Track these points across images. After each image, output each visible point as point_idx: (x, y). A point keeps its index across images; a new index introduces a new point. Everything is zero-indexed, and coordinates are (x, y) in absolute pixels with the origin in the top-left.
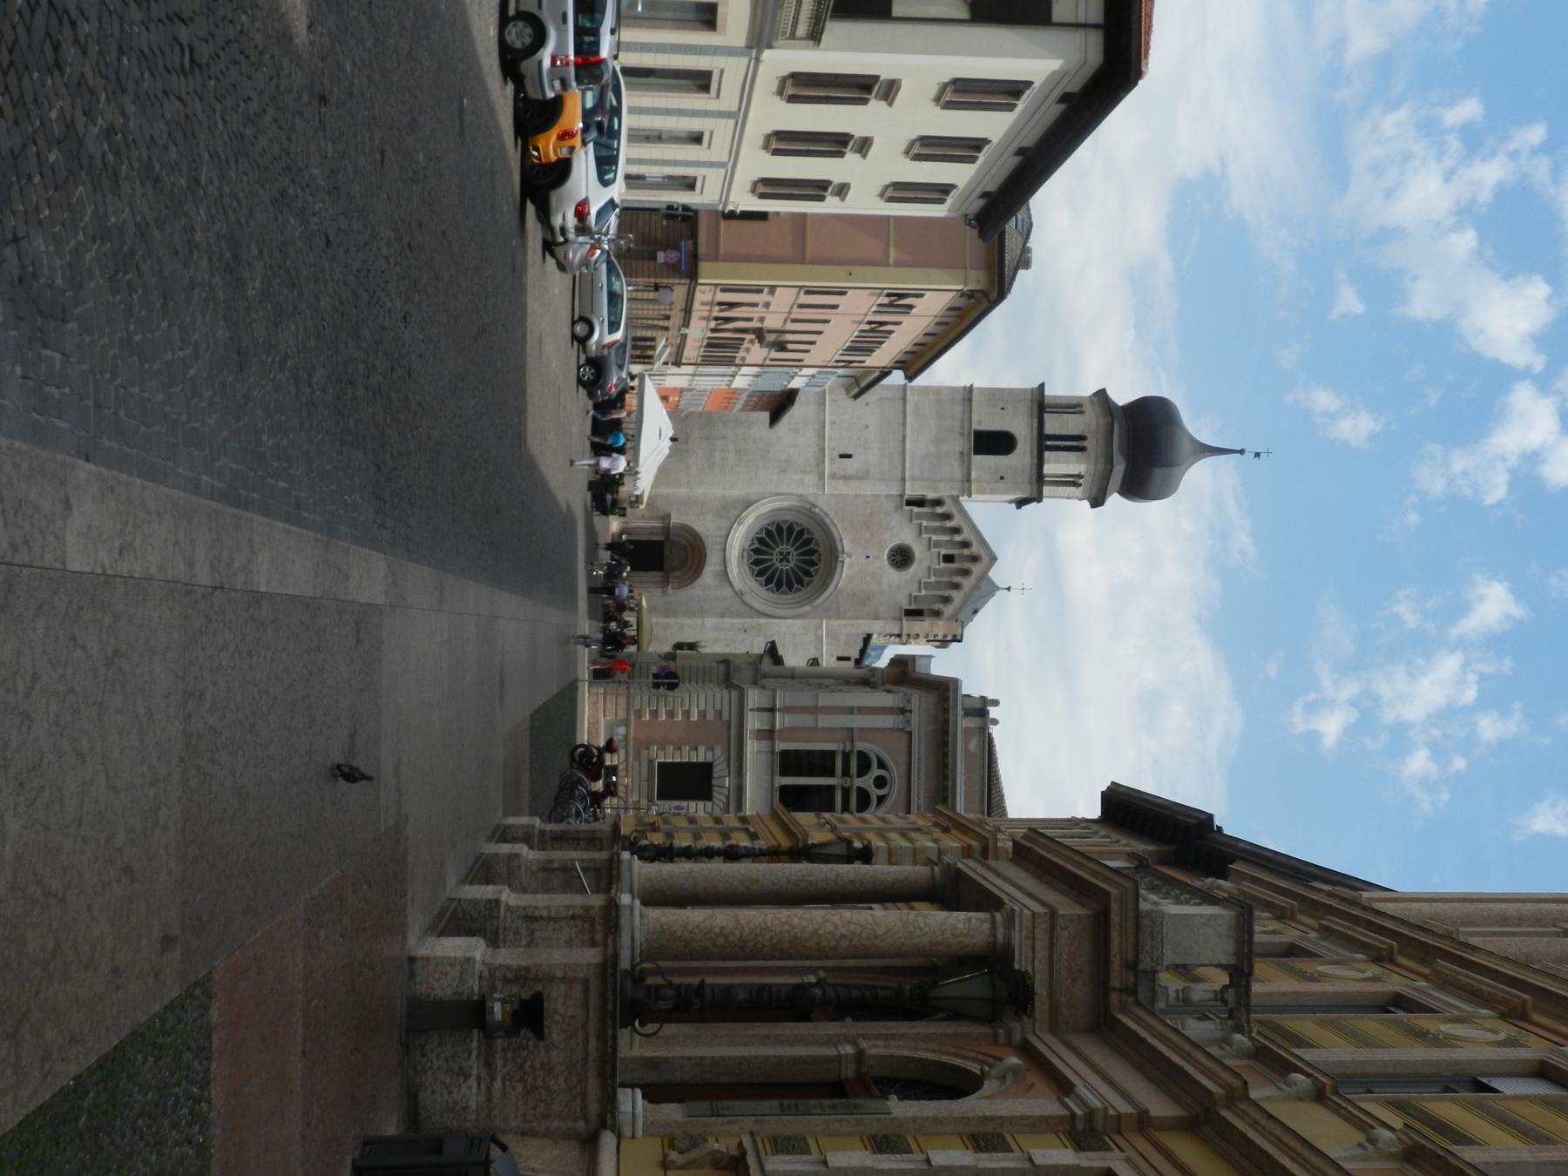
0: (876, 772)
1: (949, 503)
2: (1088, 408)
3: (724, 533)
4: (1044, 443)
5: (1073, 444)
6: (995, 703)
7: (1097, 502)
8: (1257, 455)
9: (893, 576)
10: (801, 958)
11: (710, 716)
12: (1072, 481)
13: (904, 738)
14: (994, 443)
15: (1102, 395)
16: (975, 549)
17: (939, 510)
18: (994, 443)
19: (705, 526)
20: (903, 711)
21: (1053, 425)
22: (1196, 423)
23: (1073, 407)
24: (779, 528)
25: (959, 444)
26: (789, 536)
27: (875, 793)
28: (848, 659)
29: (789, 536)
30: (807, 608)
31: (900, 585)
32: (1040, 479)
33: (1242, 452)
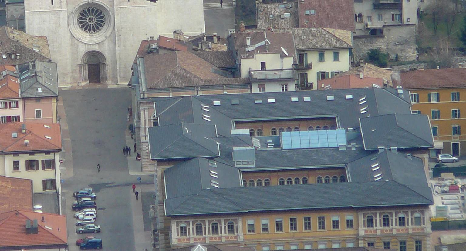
3: (84, 45)
13: (150, 109)
19: (82, 50)
26: (84, 19)
29: (84, 19)
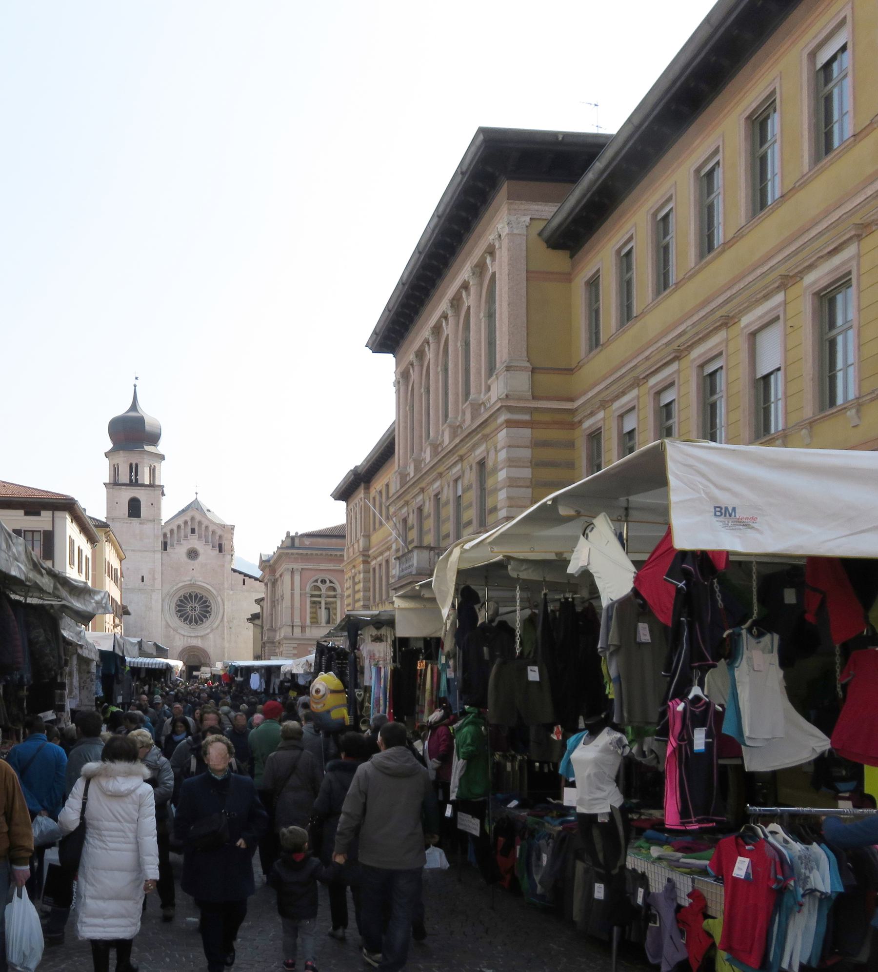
0: (319, 584)
1: (164, 530)
2: (116, 462)
4: (134, 483)
5: (134, 469)
6: (288, 533)
7: (162, 457)
8: (136, 378)
9: (201, 559)
10: (480, 350)
11: (295, 652)
12: (153, 471)
14: (134, 509)
15: (107, 455)
16: (188, 519)
17: (169, 535)
18: (134, 509)
20: (292, 572)
21: (124, 478)
22: (121, 409)
23: (115, 470)
24: (179, 611)
25: (135, 520)
27: (328, 584)
28: (244, 580)
30: (219, 598)
31: (207, 553)
32: (152, 486)
33: (135, 386)
